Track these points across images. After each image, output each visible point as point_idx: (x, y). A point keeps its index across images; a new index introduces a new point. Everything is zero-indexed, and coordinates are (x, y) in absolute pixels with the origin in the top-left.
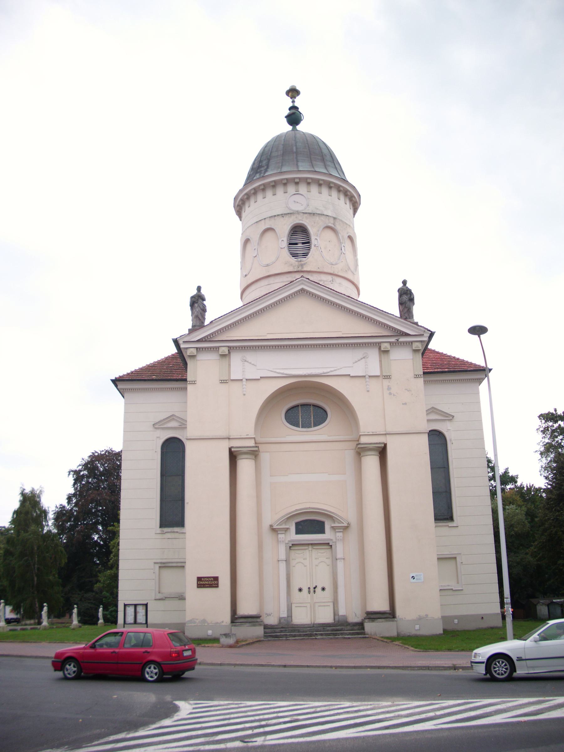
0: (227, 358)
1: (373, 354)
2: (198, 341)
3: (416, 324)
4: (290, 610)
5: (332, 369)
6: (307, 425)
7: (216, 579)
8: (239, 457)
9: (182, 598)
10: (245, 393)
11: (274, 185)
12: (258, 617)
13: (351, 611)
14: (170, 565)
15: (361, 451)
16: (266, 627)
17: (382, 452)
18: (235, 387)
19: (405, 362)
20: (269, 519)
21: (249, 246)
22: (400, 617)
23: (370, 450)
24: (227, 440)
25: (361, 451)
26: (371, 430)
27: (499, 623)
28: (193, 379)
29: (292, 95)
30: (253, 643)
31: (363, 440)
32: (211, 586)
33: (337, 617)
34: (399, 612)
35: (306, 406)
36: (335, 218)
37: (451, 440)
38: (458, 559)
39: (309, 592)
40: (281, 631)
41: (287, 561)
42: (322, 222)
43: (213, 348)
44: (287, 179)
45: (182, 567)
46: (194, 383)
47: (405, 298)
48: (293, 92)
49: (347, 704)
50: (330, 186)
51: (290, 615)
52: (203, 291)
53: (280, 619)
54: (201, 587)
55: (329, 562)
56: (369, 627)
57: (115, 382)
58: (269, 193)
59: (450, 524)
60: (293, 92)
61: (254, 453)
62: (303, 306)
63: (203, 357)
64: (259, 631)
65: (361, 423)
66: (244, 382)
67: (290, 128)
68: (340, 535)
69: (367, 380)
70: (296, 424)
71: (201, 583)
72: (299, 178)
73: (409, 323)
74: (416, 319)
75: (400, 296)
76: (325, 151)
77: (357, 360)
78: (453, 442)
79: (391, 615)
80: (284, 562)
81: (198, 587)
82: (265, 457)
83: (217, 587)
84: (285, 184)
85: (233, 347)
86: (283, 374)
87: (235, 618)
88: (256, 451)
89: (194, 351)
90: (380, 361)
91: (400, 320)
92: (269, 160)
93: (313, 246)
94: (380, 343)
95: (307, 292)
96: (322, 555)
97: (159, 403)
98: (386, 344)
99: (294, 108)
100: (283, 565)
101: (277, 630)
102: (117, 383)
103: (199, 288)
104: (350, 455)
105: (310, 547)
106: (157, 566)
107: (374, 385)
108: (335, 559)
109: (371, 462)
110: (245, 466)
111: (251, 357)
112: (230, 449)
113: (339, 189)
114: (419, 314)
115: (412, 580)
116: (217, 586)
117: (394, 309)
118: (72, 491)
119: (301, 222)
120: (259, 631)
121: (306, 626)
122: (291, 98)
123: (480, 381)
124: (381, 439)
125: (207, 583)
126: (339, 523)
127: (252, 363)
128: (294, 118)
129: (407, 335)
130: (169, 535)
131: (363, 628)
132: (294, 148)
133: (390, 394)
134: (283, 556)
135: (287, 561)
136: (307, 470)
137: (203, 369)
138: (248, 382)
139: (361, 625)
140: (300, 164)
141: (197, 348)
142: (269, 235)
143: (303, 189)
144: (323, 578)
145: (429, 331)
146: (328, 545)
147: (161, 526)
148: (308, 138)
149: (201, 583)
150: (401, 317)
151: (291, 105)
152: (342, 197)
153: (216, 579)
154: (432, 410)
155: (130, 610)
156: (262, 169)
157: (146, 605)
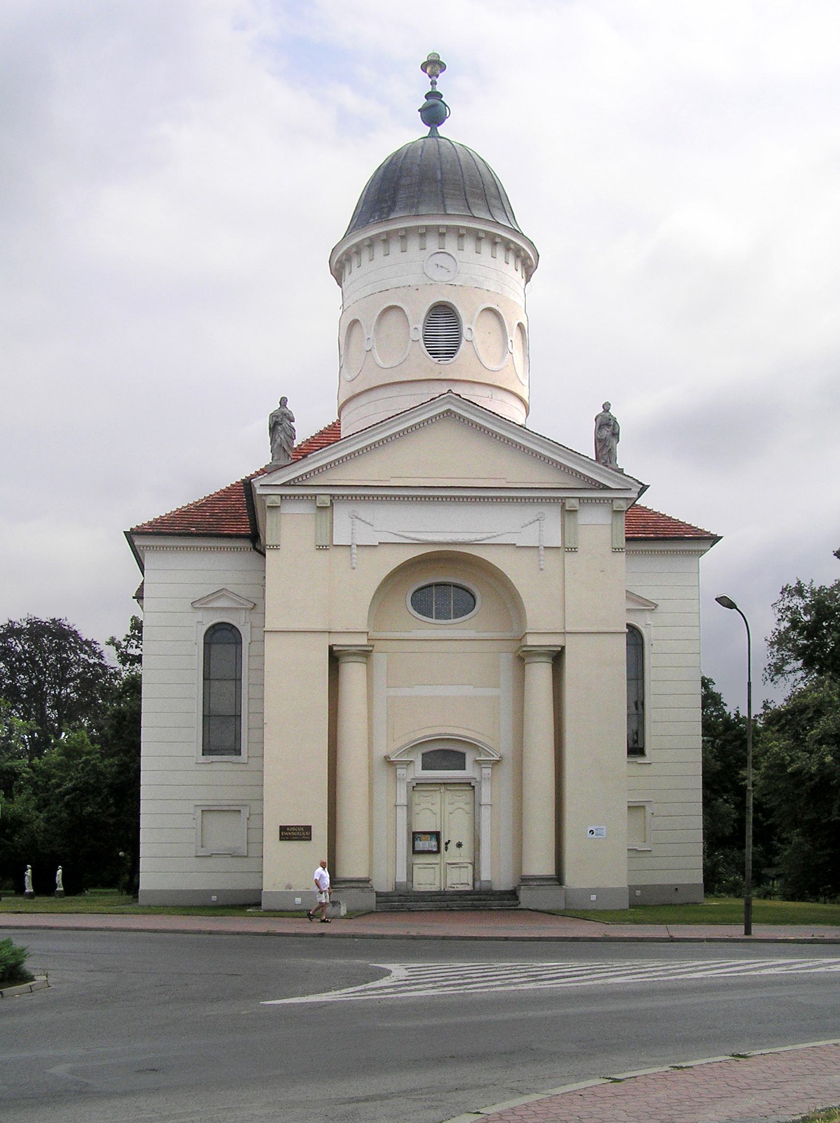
0: (329, 512)
1: (552, 518)
2: (283, 485)
3: (621, 471)
5: (489, 535)
6: (442, 615)
7: (308, 829)
8: (342, 660)
10: (354, 565)
11: (404, 235)
12: (367, 881)
13: (496, 873)
15: (523, 657)
16: (378, 894)
17: (557, 658)
18: (340, 556)
19: (598, 527)
20: (382, 749)
21: (356, 331)
23: (540, 654)
24: (327, 634)
25: (523, 657)
26: (543, 627)
29: (431, 71)
30: (363, 915)
31: (531, 641)
32: (300, 838)
33: (477, 885)
34: (570, 879)
35: (443, 584)
38: (647, 808)
44: (427, 227)
46: (276, 547)
47: (606, 432)
48: (434, 66)
49: (576, 964)
50: (494, 241)
55: (467, 808)
56: (526, 898)
59: (640, 760)
60: (434, 66)
61: (365, 654)
62: (447, 434)
63: (289, 509)
64: (370, 901)
65: (529, 616)
66: (355, 550)
68: (487, 771)
69: (542, 552)
70: (426, 613)
71: (286, 834)
72: (447, 227)
73: (610, 471)
74: (620, 463)
76: (488, 179)
77: (527, 522)
78: (654, 642)
79: (558, 878)
80: (405, 808)
81: (281, 839)
82: (379, 659)
83: (310, 839)
84: (422, 235)
85: (338, 496)
86: (413, 539)
88: (371, 651)
90: (563, 526)
91: (597, 464)
92: (396, 190)
93: (463, 341)
95: (456, 414)
96: (461, 800)
98: (573, 501)
99: (433, 95)
100: (402, 813)
103: (283, 402)
104: (506, 661)
105: (443, 789)
107: (551, 561)
108: (476, 806)
109: (540, 674)
110: (353, 674)
111: (365, 511)
112: (331, 648)
113: (508, 246)
114: (626, 456)
116: (309, 838)
117: (585, 444)
119: (446, 300)
120: (370, 901)
122: (430, 77)
124: (556, 641)
125: (294, 834)
126: (487, 756)
127: (368, 521)
128: (433, 113)
129: (606, 488)
132: (439, 172)
134: (402, 800)
135: (409, 807)
136: (443, 682)
137: (290, 529)
138: (360, 549)
139: (513, 894)
141: (282, 496)
142: (393, 317)
143: (451, 244)
145: (641, 483)
146: (469, 785)
147: (207, 750)
148: (461, 156)
149: (286, 834)
150: (598, 459)
151: (430, 90)
152: (511, 258)
153: (308, 829)
154: (630, 596)
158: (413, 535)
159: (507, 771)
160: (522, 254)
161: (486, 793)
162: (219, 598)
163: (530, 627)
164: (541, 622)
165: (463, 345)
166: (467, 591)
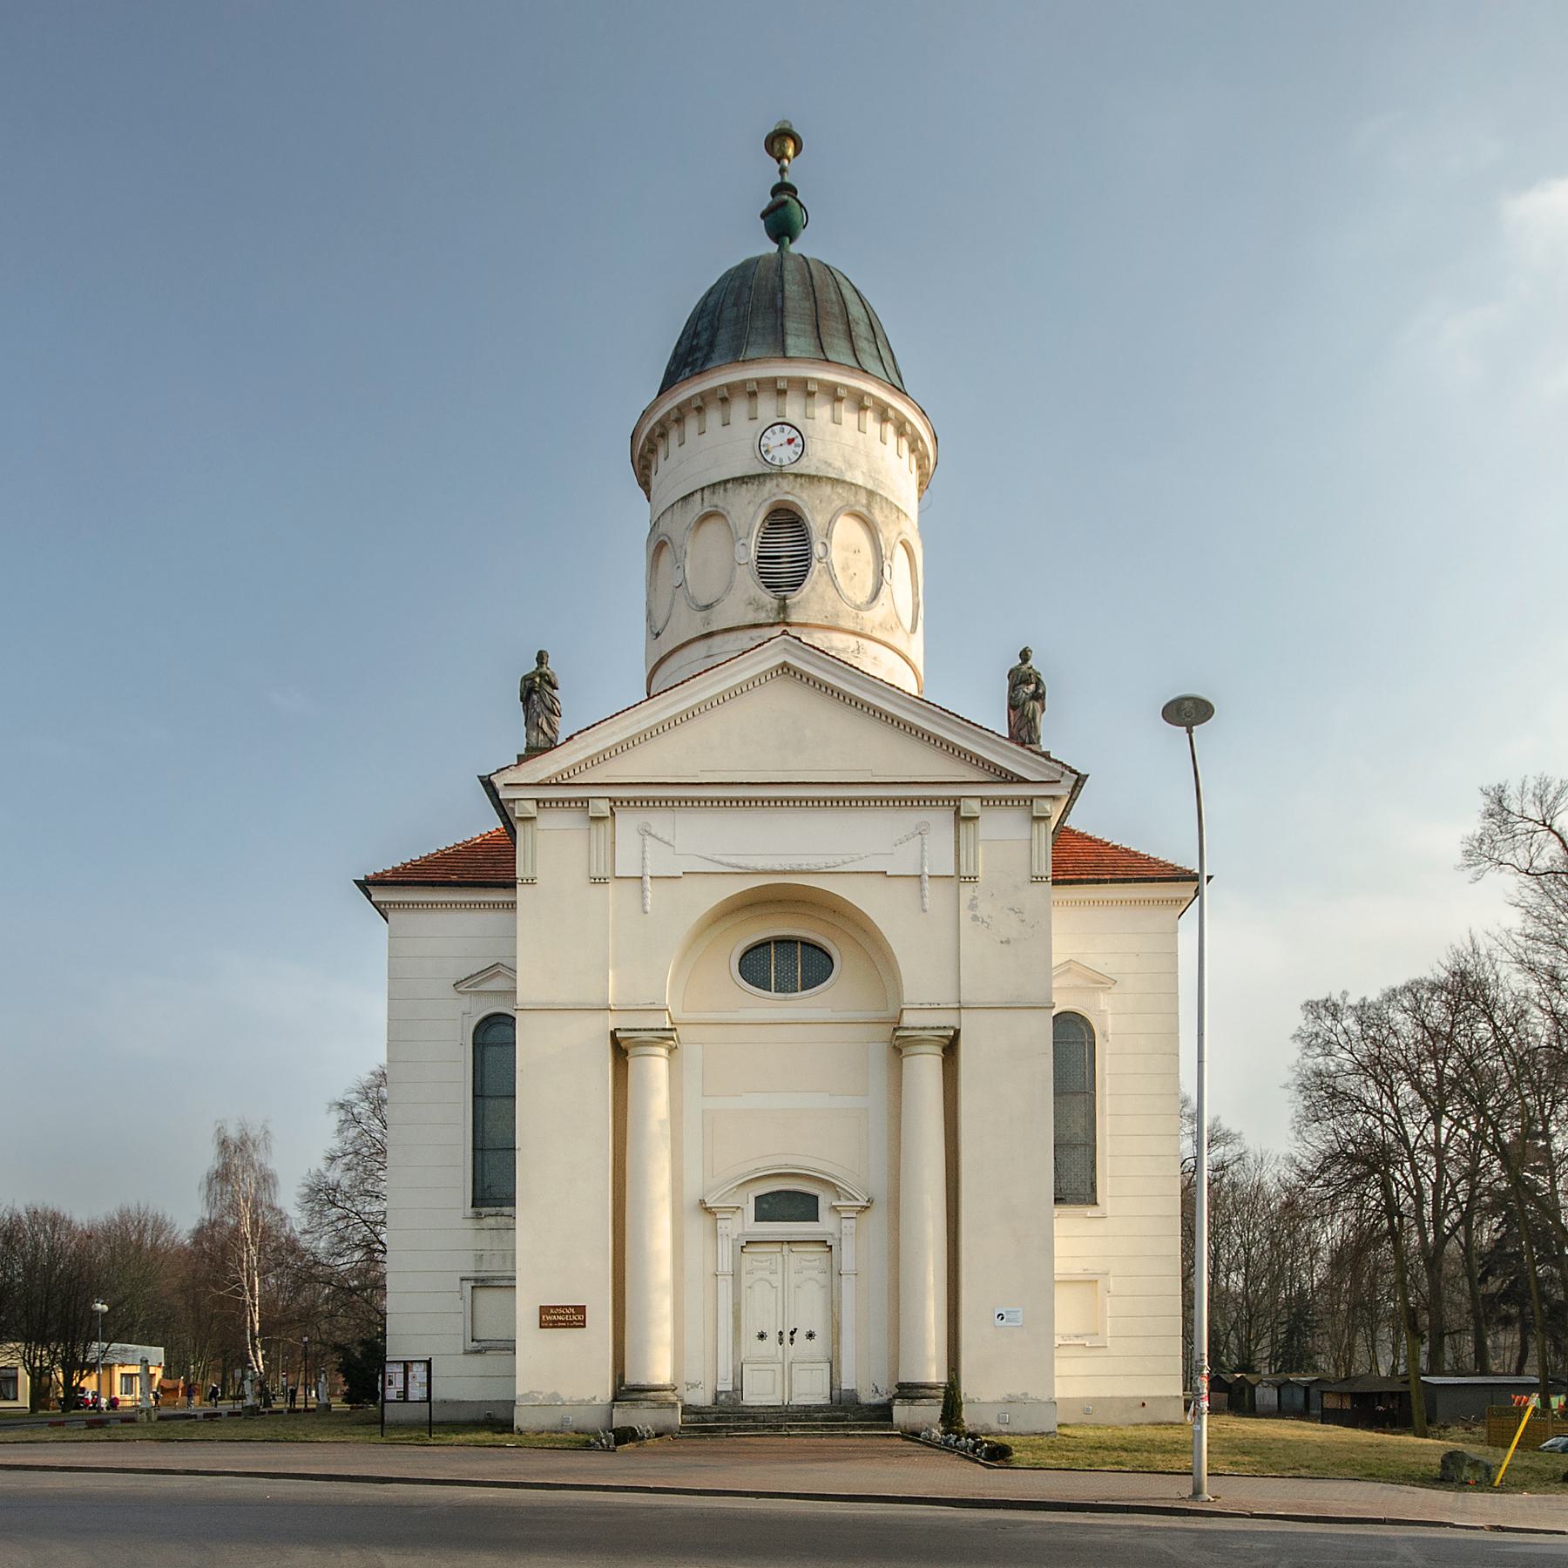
0: (609, 823)
1: (941, 820)
3: (1046, 755)
4: (739, 1375)
7: (581, 1310)
9: (509, 1347)
13: (864, 1379)
14: (496, 1283)
15: (900, 1045)
16: (687, 1409)
17: (950, 1048)
19: (1008, 845)
21: (666, 558)
22: (969, 1396)
25: (900, 1045)
26: (927, 997)
27: (1176, 1412)
28: (529, 875)
32: (569, 1325)
36: (871, 494)
37: (1104, 1035)
39: (781, 1341)
40: (718, 1419)
41: (736, 1275)
42: (838, 497)
43: (576, 800)
45: (508, 1284)
46: (531, 882)
51: (739, 1389)
52: (552, 666)
53: (717, 1394)
54: (555, 1325)
57: (366, 885)
58: (713, 417)
59: (1090, 1211)
61: (665, 1036)
67: (774, 248)
75: (1013, 687)
86: (728, 865)
87: (625, 1392)
89: (531, 808)
92: (714, 329)
93: (814, 561)
94: (957, 799)
97: (452, 930)
100: (725, 1286)
101: (708, 1417)
102: (371, 889)
103: (541, 658)
104: (879, 1052)
106: (468, 1285)
108: (835, 1273)
109: (926, 1067)
110: (655, 1068)
111: (658, 821)
112: (613, 1034)
114: (1054, 734)
115: (998, 1321)
117: (997, 720)
118: (335, 1144)
119: (790, 498)
121: (463, 1415)
123: (1182, 905)
124: (947, 1019)
128: (781, 219)
130: (491, 1221)
131: (889, 1417)
133: (975, 918)
134: (726, 1265)
135: (736, 1275)
137: (550, 851)
140: (790, 341)
141: (538, 801)
142: (712, 527)
144: (809, 1313)
145: (1074, 772)
151: (778, 180)
153: (581, 1310)
155: (418, 1371)
156: (699, 355)
157: (429, 1363)
158: (734, 860)
159: (877, 1220)
160: (908, 428)
161: (848, 1256)
162: (493, 976)
163: (910, 995)
164: (923, 988)
165: (816, 567)
166: (821, 950)
